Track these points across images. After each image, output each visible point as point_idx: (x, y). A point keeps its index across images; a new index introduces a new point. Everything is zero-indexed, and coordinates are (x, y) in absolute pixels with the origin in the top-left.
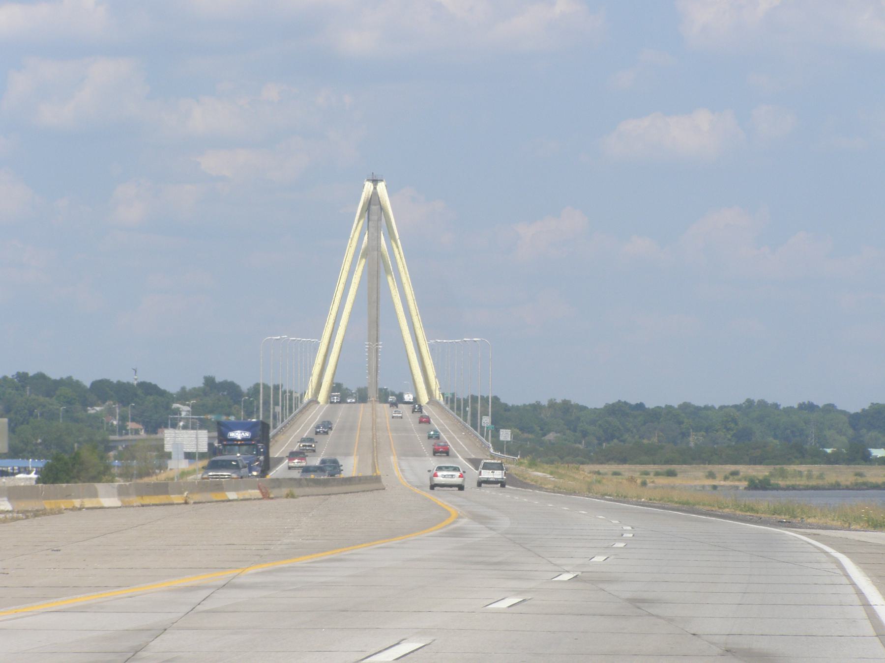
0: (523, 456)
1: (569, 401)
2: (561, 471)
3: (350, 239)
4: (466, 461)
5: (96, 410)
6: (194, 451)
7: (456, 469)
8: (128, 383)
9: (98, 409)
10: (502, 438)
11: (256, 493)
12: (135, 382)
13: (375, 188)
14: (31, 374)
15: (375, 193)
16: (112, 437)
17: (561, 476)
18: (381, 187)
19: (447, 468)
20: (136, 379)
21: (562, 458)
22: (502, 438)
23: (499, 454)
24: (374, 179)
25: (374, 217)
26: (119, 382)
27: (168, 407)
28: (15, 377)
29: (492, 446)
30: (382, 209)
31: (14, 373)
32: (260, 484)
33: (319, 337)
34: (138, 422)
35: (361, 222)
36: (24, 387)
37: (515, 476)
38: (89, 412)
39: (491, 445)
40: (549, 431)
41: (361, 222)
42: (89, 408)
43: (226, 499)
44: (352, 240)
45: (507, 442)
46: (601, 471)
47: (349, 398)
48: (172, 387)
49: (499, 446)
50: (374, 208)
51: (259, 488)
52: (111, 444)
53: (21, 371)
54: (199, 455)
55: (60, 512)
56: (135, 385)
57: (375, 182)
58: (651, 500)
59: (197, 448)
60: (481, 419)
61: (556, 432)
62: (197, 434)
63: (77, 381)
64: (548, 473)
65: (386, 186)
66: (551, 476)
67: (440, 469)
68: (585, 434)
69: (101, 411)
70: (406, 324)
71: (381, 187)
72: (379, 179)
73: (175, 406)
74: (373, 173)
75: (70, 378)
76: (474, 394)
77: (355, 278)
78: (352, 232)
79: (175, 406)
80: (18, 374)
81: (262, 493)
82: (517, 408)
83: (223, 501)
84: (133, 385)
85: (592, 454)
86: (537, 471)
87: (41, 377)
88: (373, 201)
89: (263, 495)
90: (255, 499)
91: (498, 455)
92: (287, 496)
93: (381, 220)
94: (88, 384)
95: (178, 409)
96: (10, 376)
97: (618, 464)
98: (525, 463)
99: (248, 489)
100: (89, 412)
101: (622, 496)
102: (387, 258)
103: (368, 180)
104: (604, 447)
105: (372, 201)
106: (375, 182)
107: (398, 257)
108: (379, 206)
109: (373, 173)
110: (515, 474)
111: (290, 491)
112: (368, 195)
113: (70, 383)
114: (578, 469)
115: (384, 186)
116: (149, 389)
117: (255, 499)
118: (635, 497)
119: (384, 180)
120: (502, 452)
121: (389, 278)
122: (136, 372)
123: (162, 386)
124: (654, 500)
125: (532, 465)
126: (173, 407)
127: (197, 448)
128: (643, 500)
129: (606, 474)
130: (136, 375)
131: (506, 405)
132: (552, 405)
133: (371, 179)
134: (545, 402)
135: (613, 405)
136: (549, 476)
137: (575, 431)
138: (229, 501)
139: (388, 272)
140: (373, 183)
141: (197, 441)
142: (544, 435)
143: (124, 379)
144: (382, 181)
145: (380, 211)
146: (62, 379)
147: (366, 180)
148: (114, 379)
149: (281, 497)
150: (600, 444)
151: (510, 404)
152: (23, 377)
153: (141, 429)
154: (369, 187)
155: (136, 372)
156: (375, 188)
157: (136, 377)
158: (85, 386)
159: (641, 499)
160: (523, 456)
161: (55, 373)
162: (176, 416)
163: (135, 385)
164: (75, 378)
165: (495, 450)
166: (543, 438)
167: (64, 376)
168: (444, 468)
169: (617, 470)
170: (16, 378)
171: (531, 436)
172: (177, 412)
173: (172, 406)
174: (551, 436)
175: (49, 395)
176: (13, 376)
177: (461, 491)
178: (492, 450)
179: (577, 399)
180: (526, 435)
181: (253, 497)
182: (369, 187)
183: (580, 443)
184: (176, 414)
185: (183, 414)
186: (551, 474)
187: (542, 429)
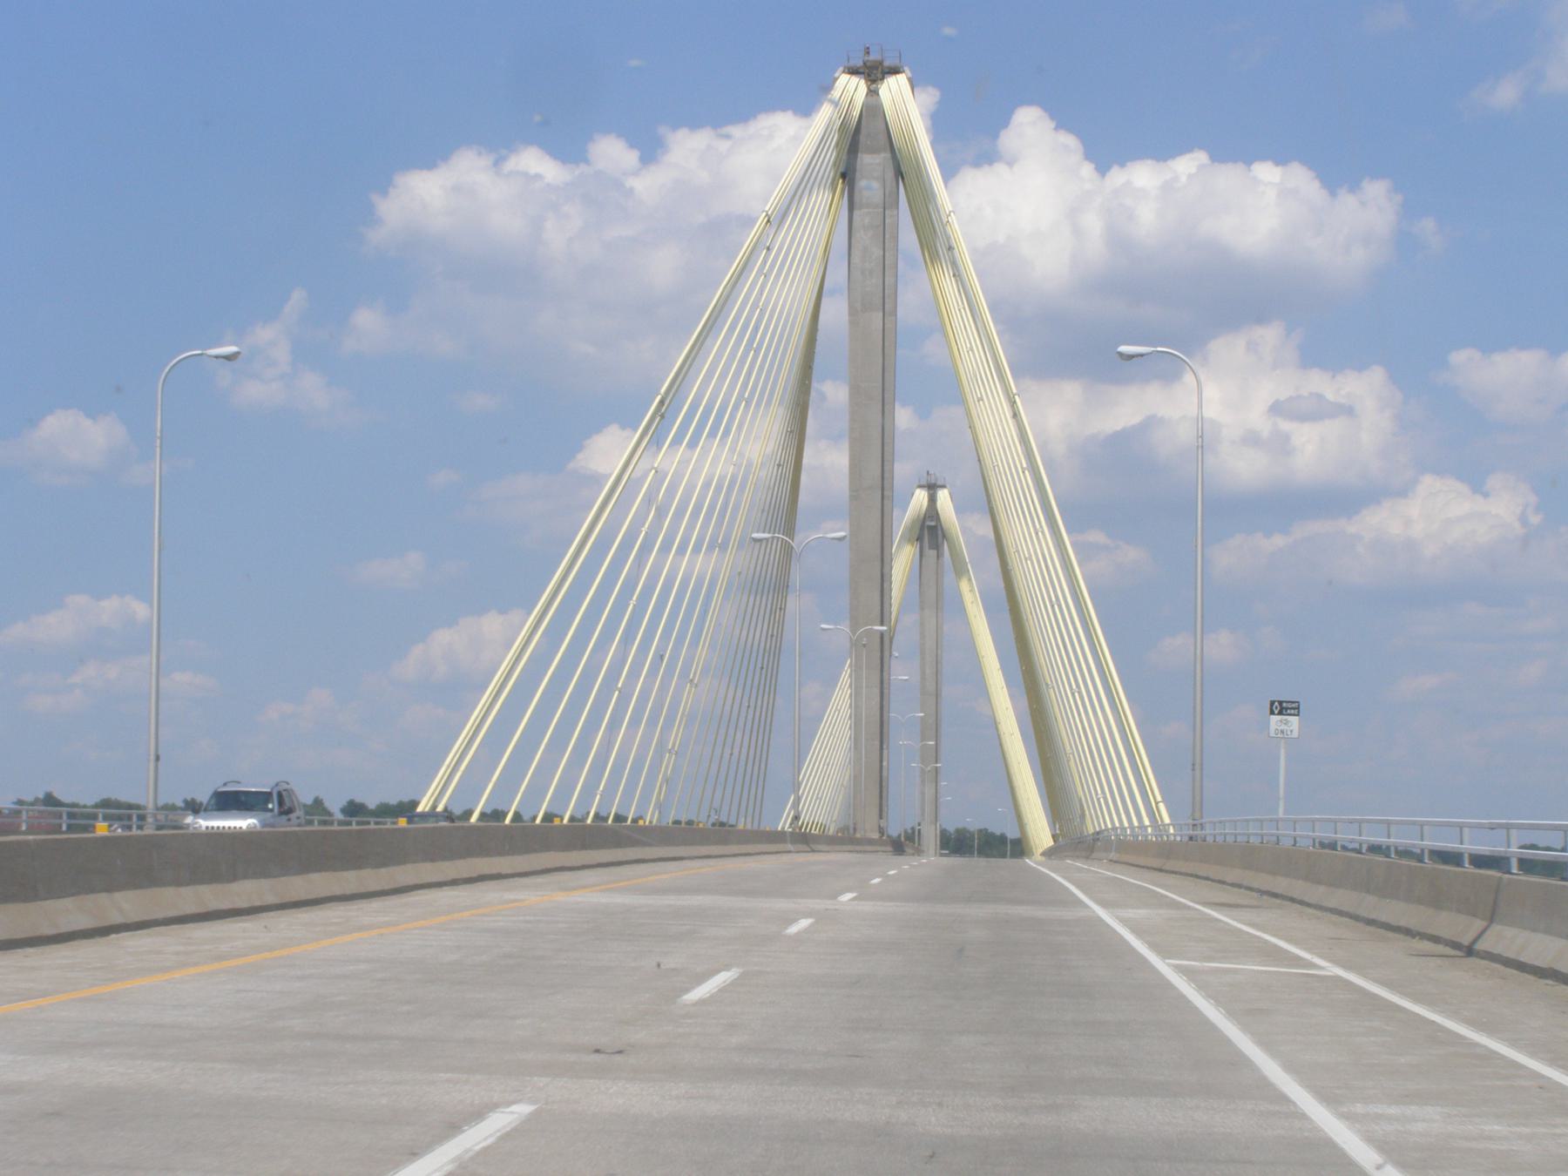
13: (872, 93)
25: (870, 187)
50: (872, 163)
54: (1006, 854)
55: (878, 851)
57: (874, 73)
59: (728, 819)
70: (998, 666)
71: (894, 89)
72: (939, 483)
74: (928, 472)
76: (341, 806)
102: (958, 538)
105: (862, 138)
106: (874, 73)
108: (888, 155)
109: (928, 472)
119: (906, 69)
121: (964, 586)
127: (728, 819)
147: (841, 69)
154: (851, 89)
156: (872, 93)
177: (1016, 860)
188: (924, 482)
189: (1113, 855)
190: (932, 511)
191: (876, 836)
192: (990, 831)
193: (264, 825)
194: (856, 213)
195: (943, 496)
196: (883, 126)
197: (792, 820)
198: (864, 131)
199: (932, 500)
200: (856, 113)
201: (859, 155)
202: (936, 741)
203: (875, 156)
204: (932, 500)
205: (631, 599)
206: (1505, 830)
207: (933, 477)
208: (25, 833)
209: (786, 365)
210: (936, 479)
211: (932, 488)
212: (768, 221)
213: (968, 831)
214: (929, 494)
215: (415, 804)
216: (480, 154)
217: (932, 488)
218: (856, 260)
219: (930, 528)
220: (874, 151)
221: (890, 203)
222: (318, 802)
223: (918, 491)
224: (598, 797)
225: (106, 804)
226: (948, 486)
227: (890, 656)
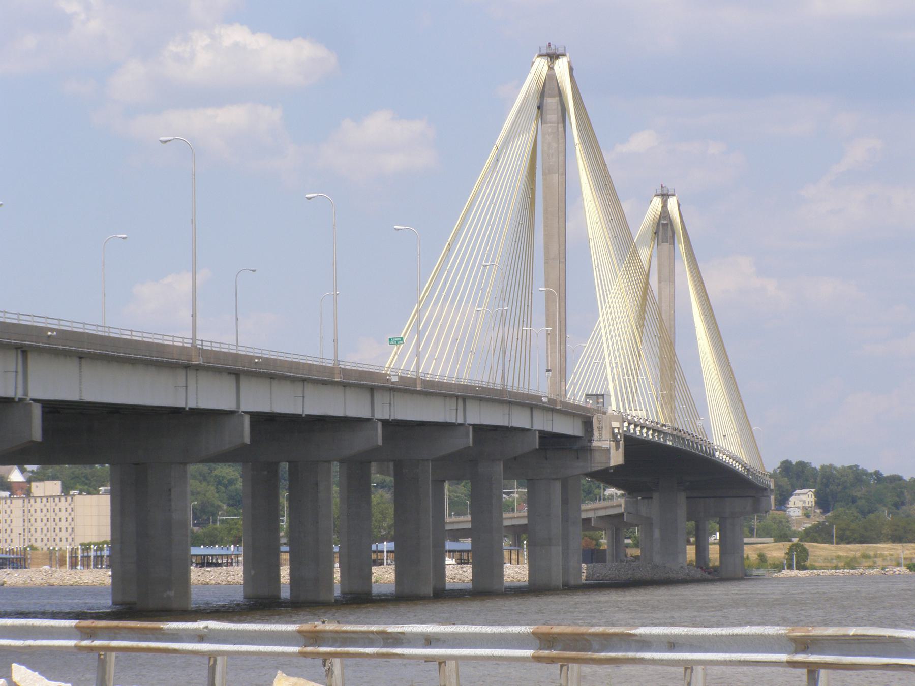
13: (551, 68)
15: (551, 77)
30: (560, 94)
50: (551, 102)
57: (553, 57)
59: (552, 429)
71: (561, 67)
103: (541, 56)
108: (557, 98)
109: (662, 186)
127: (552, 429)
154: (541, 66)
156: (551, 68)
190: (665, 213)
192: (860, 468)
195: (672, 203)
196: (556, 84)
197: (551, 408)
198: (547, 86)
199: (665, 205)
201: (545, 98)
203: (553, 99)
204: (665, 205)
205: (443, 292)
206: (239, 344)
207: (665, 189)
209: (516, 189)
210: (668, 190)
211: (665, 196)
212: (497, 149)
213: (835, 468)
214: (662, 200)
216: (515, 599)
217: (665, 196)
219: (664, 225)
220: (552, 96)
223: (655, 198)
224: (439, 325)
226: (676, 195)
227: (566, 338)
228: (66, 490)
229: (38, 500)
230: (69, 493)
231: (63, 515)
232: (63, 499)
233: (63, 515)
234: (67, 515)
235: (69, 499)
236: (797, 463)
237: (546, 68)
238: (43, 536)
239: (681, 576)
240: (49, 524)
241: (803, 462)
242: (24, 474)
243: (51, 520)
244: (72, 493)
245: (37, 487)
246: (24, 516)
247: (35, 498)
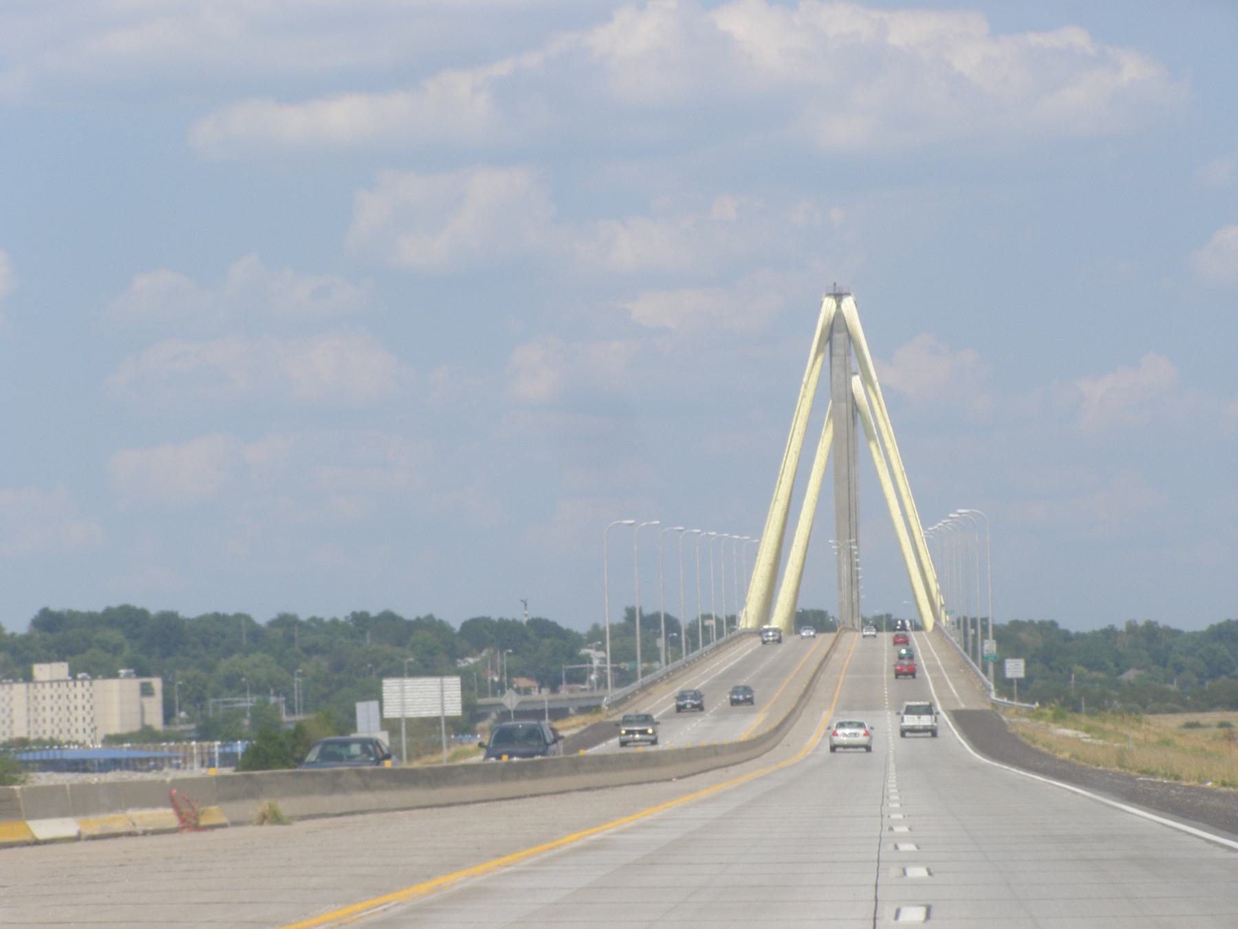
0: (1042, 705)
1: (1156, 623)
2: (1109, 726)
3: (803, 386)
4: (948, 716)
5: (469, 663)
6: (436, 713)
7: (861, 725)
8: (514, 621)
9: (471, 660)
10: (1009, 675)
11: (165, 816)
12: (525, 620)
13: (839, 307)
14: (374, 613)
15: (839, 315)
16: (481, 701)
17: (1104, 734)
18: (848, 305)
19: (850, 724)
20: (526, 615)
21: (1144, 705)
22: (1009, 675)
23: (1005, 700)
24: (837, 291)
25: (839, 351)
26: (501, 620)
27: (572, 656)
28: (350, 618)
29: (996, 687)
30: (850, 337)
31: (348, 613)
32: (174, 791)
33: (759, 532)
34: (529, 677)
35: (820, 359)
36: (363, 633)
37: (1024, 739)
38: (459, 666)
39: (992, 687)
40: (1128, 667)
41: (820, 359)
42: (459, 660)
43: (28, 838)
44: (806, 387)
45: (1019, 680)
46: (1202, 722)
47: (805, 629)
48: (581, 627)
49: (1005, 686)
50: (839, 337)
51: (173, 803)
52: (480, 711)
53: (358, 610)
56: (524, 623)
57: (839, 296)
58: (1224, 784)
60: (982, 645)
61: (1138, 669)
62: (442, 681)
63: (441, 622)
64: (1081, 730)
65: (855, 303)
66: (1087, 735)
67: (842, 725)
68: (1179, 669)
69: (476, 663)
71: (848, 305)
72: (844, 291)
73: (584, 651)
74: (835, 284)
75: (430, 617)
77: (822, 448)
78: (807, 371)
79: (584, 651)
80: (354, 614)
81: (179, 814)
82: (1080, 636)
83: (27, 844)
84: (520, 624)
85: (1189, 698)
86: (1065, 727)
87: (389, 618)
88: (837, 325)
89: (183, 820)
90: (145, 833)
91: (1005, 703)
92: (263, 819)
93: (850, 355)
94: (457, 626)
95: (588, 655)
96: (341, 618)
97: (1228, 710)
98: (1046, 715)
99: (124, 809)
100: (459, 666)
101: (1171, 775)
103: (829, 295)
104: (1207, 687)
105: (835, 326)
106: (839, 296)
107: (878, 414)
109: (835, 284)
110: (1024, 735)
111: (270, 806)
112: (830, 315)
113: (431, 625)
114: (1139, 721)
115: (853, 303)
116: (543, 628)
117: (145, 833)
118: (1194, 779)
119: (853, 294)
120: (1011, 697)
121: (873, 446)
122: (526, 605)
123: (564, 623)
124: (1230, 785)
125: (1058, 718)
126: (580, 654)
128: (1209, 784)
129: (1209, 726)
130: (526, 609)
131: (1066, 632)
132: (1132, 628)
133: (832, 292)
134: (1121, 626)
135: (1220, 626)
136: (1081, 735)
137: (1164, 665)
138: (37, 843)
139: (870, 436)
140: (835, 298)
141: (442, 695)
142: (1121, 673)
143: (509, 616)
144: (849, 294)
145: (847, 341)
146: (418, 619)
147: (824, 294)
148: (495, 617)
149: (250, 823)
150: (1202, 683)
151: (1073, 630)
152: (361, 620)
153: (535, 687)
154: (829, 305)
155: (526, 605)
156: (839, 307)
157: (526, 612)
158: (453, 629)
159: (1205, 782)
160: (1042, 705)
161: (408, 612)
162: (584, 666)
163: (524, 623)
164: (437, 617)
165: (1000, 694)
166: (1119, 678)
167: (422, 614)
168: (846, 724)
169: (79, 720)
170: (352, 620)
171: (1101, 675)
172: (587, 659)
173: (580, 651)
174: (1130, 675)
175: (400, 643)
176: (346, 618)
178: (993, 696)
179: (1165, 619)
180: (1095, 674)
181: (139, 829)
182: (829, 305)
183: (1172, 682)
184: (585, 662)
185: (596, 663)
186: (1088, 730)
187: (1117, 665)
188: (831, 291)
189: (690, 641)
191: (851, 627)
193: (946, 627)
194: (834, 359)
200: (832, 317)
202: (856, 538)
208: (976, 631)
215: (732, 620)
218: (834, 379)
221: (847, 354)
222: (596, 627)
225: (48, 621)
228: (73, 674)
229: (47, 685)
230: (455, 664)
231: (80, 702)
232: (71, 684)
233: (80, 702)
234: (84, 702)
235: (79, 683)
236: (466, 626)
237: (835, 305)
238: (85, 725)
239: (833, 351)
240: (61, 714)
241: (217, 617)
242: (896, 647)
243: (64, 709)
244: (80, 676)
245: (41, 669)
246: (28, 704)
247: (43, 683)
